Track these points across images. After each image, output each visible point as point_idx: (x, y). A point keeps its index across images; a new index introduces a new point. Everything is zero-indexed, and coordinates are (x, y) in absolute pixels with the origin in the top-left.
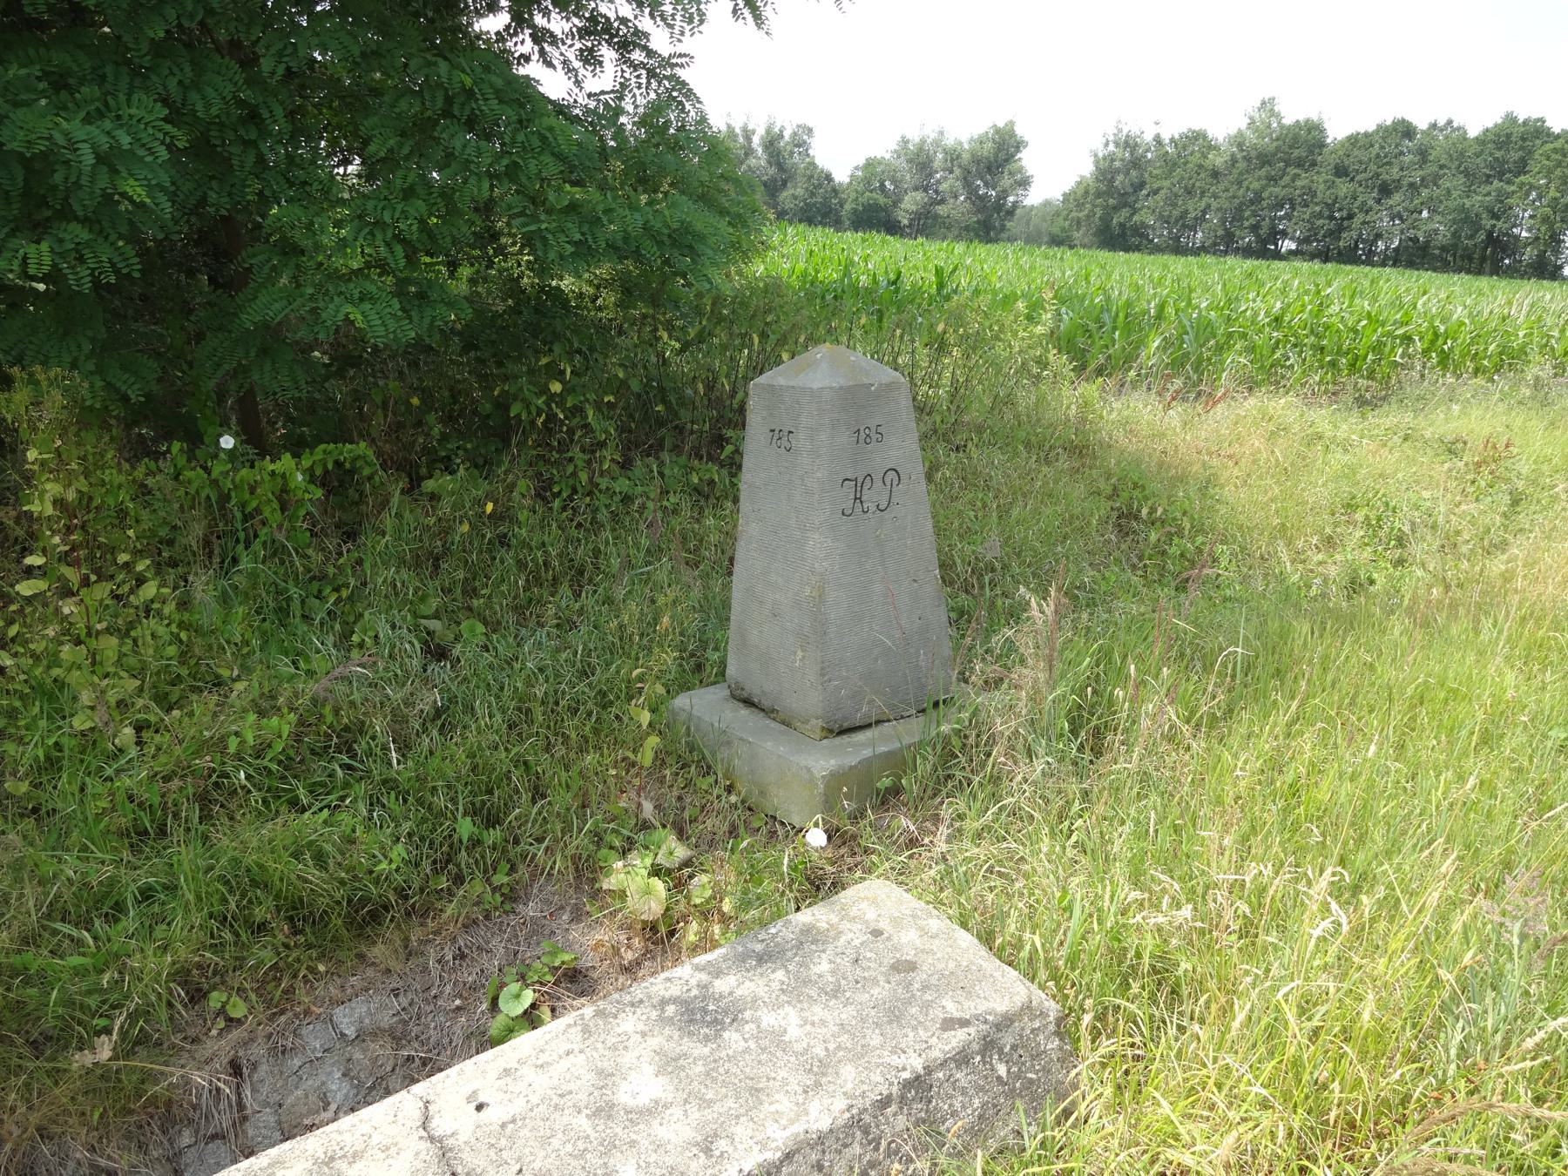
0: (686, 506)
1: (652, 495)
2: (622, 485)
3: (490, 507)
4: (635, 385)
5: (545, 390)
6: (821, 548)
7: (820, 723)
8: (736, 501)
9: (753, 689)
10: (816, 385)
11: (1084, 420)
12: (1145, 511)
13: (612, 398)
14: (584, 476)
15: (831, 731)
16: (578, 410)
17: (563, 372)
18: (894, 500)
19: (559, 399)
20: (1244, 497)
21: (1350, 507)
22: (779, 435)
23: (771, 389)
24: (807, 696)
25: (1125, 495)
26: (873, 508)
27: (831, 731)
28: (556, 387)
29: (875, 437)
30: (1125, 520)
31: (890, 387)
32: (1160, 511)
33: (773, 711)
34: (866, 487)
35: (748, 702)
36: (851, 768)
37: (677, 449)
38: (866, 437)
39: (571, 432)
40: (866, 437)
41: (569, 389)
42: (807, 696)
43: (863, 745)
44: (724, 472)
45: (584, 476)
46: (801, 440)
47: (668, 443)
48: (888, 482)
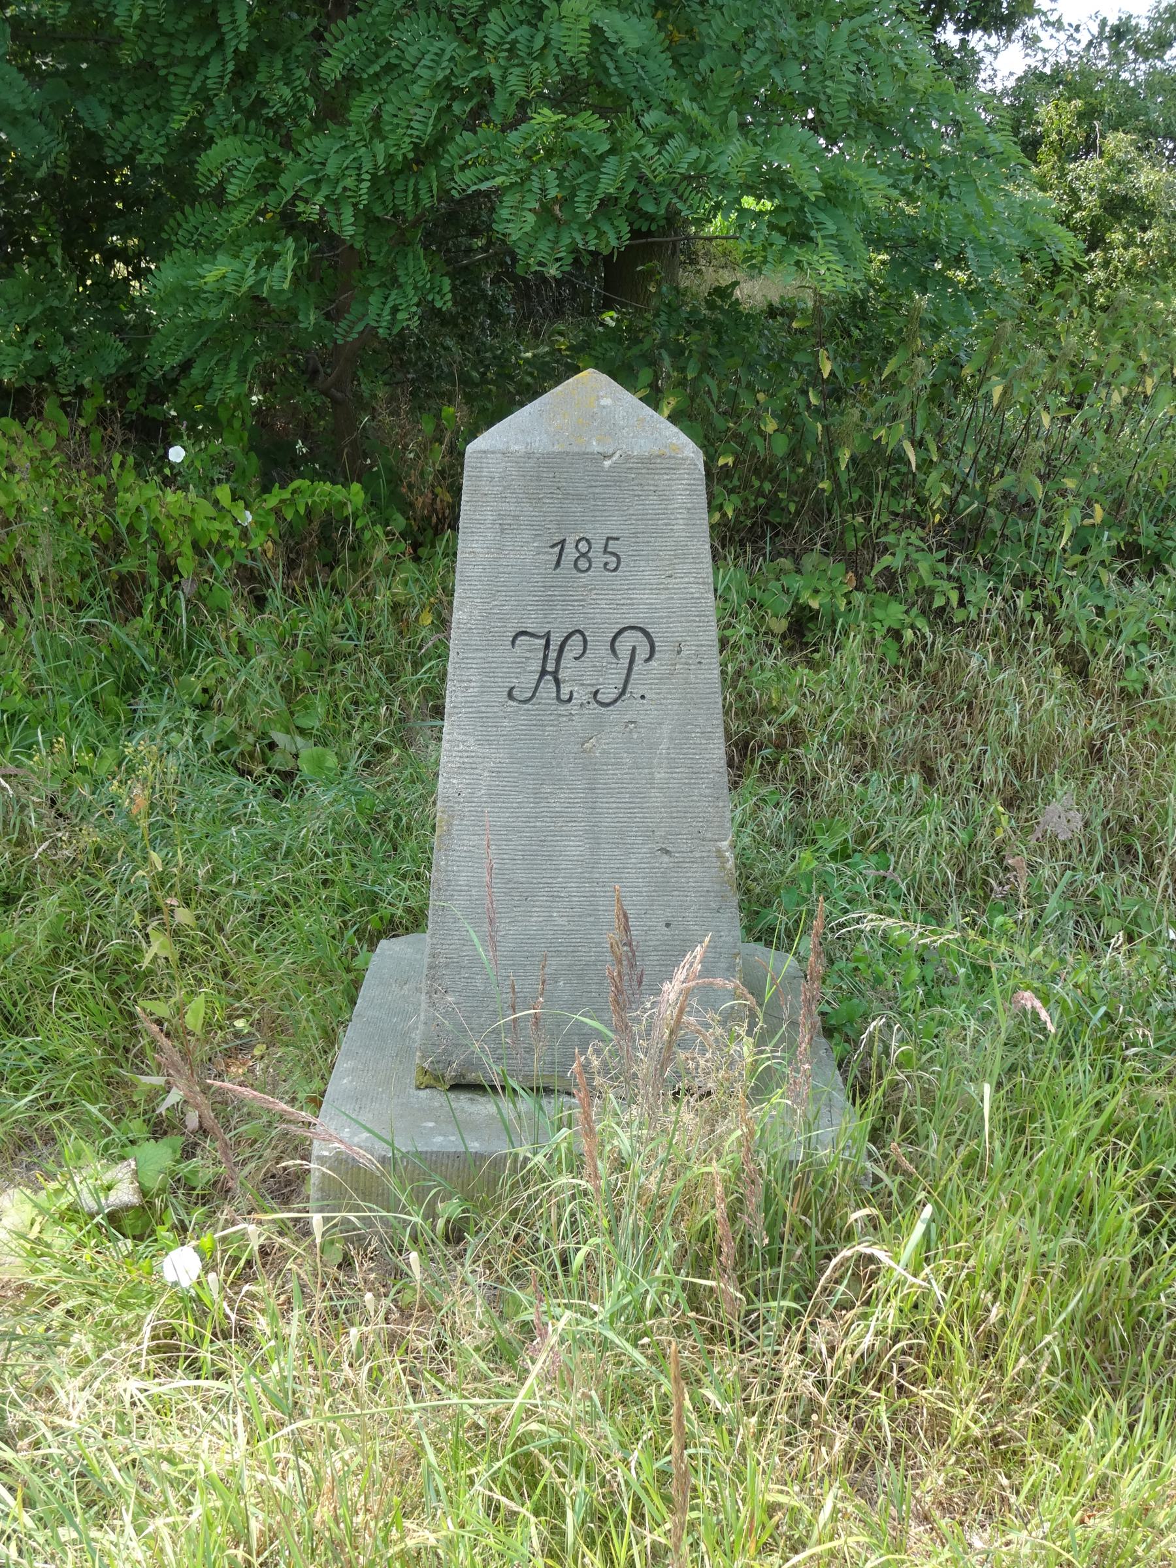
34: (568, 655)
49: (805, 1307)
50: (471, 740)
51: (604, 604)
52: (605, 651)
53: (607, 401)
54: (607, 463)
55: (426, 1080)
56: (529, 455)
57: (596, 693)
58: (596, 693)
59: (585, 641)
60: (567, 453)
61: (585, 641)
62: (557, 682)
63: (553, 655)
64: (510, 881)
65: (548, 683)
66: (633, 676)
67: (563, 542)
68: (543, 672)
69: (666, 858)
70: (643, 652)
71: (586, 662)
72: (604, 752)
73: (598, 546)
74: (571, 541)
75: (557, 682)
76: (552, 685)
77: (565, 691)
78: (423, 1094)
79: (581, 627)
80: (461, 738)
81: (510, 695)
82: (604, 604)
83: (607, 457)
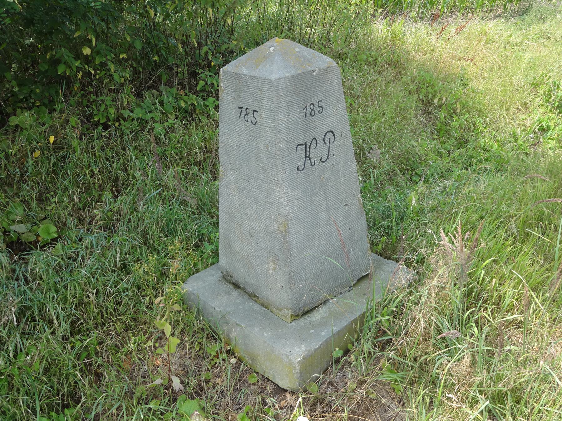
0: (178, 125)
1: (157, 119)
2: (138, 113)
3: (52, 139)
4: (138, 45)
5: (78, 56)
6: (285, 196)
7: (290, 312)
8: (215, 175)
9: (240, 275)
10: (274, 77)
11: (393, 44)
12: (436, 100)
13: (125, 56)
14: (112, 111)
15: (297, 316)
16: (103, 65)
17: (90, 41)
18: (331, 153)
19: (87, 60)
20: (484, 85)
21: (535, 86)
22: (245, 112)
23: (237, 76)
24: (279, 293)
25: (424, 91)
26: (317, 161)
27: (297, 316)
28: (87, 51)
29: (317, 109)
30: (427, 106)
31: (326, 71)
32: (444, 99)
33: (255, 296)
34: (312, 148)
35: (236, 286)
36: (316, 349)
37: (169, 84)
38: (311, 111)
39: (101, 80)
40: (311, 111)
41: (96, 52)
42: (279, 293)
43: (322, 324)
44: (200, 99)
45: (112, 111)
46: (264, 117)
47: (164, 78)
48: (327, 142)
49: (414, 285)
50: (289, 190)
51: (320, 125)
52: (322, 143)
53: (297, 50)
54: (315, 73)
55: (293, 318)
56: (292, 77)
57: (321, 159)
58: (321, 159)
59: (316, 141)
60: (303, 73)
61: (316, 141)
62: (310, 159)
63: (308, 150)
64: (308, 236)
65: (308, 161)
66: (331, 149)
67: (306, 107)
68: (306, 157)
69: (346, 207)
70: (332, 140)
71: (318, 149)
72: (327, 178)
73: (316, 105)
74: (308, 106)
75: (310, 159)
76: (309, 161)
77: (313, 161)
78: (294, 323)
79: (315, 137)
80: (286, 191)
81: (298, 170)
82: (320, 125)
83: (314, 71)
